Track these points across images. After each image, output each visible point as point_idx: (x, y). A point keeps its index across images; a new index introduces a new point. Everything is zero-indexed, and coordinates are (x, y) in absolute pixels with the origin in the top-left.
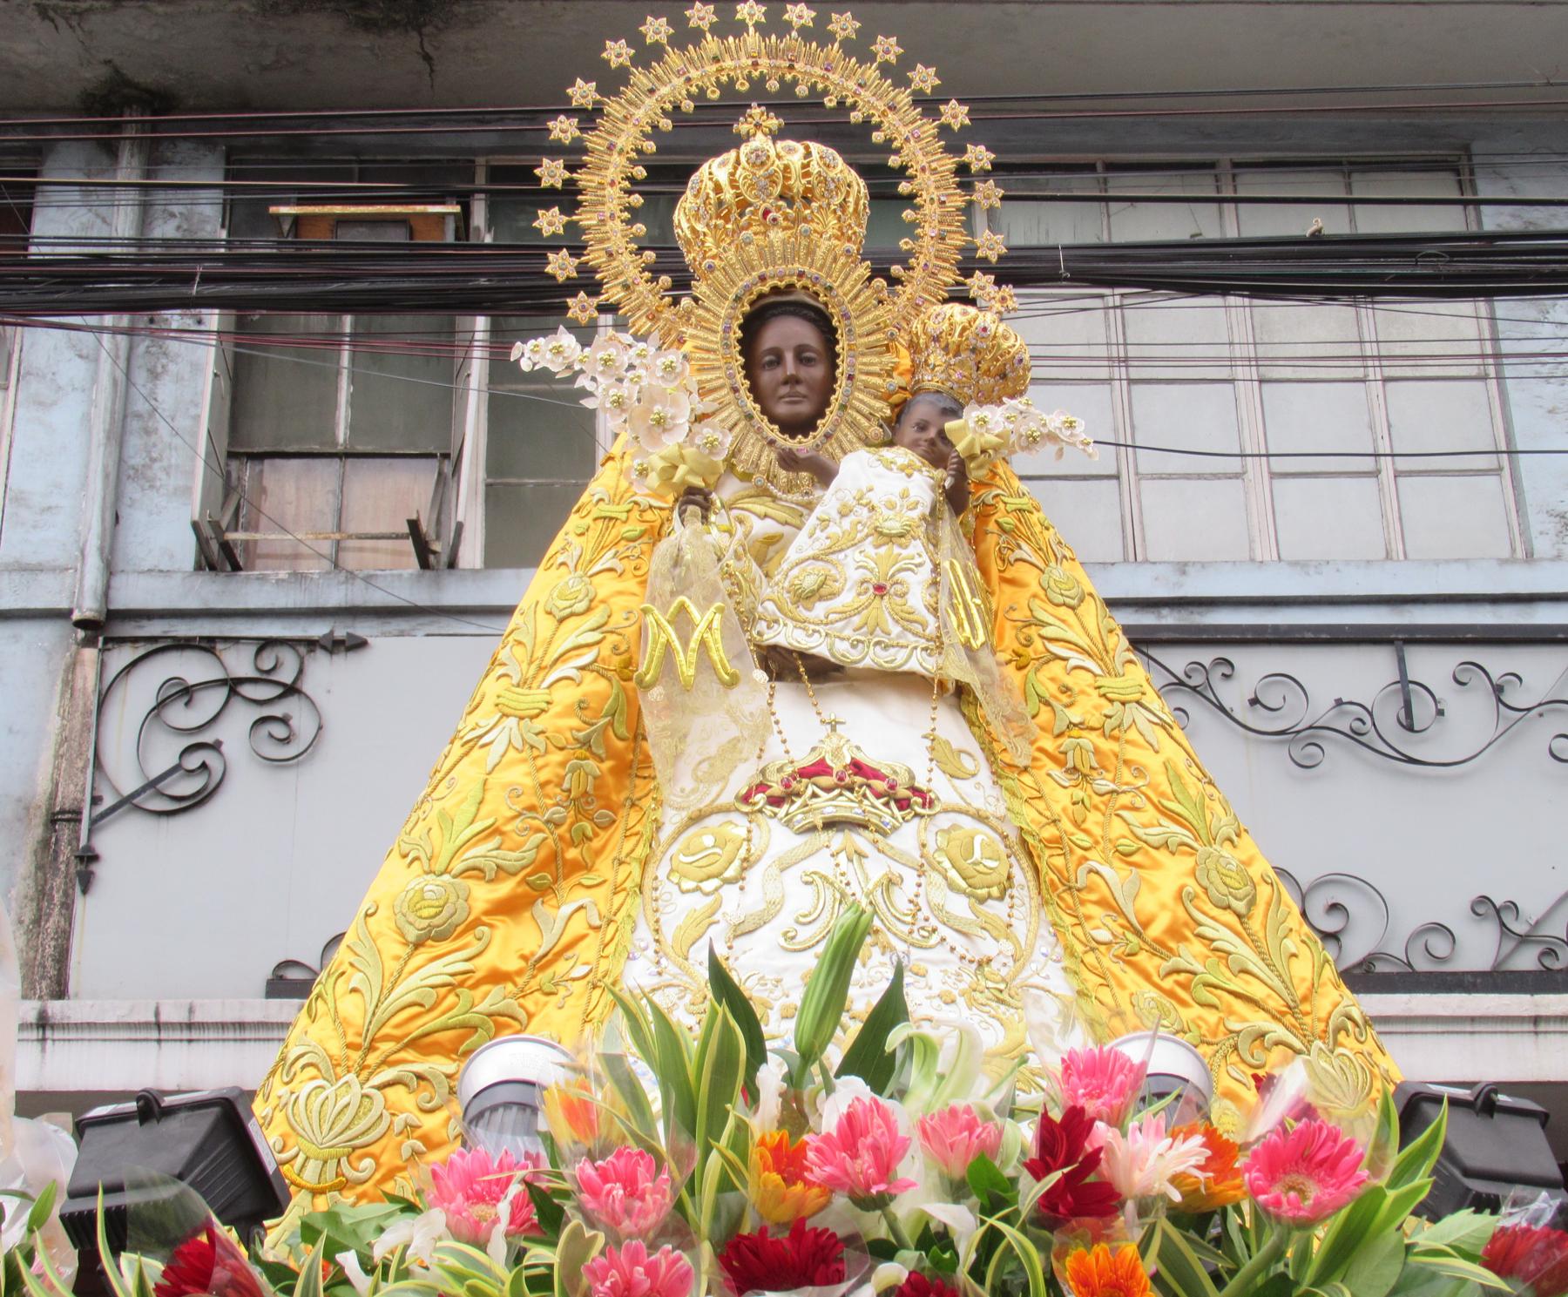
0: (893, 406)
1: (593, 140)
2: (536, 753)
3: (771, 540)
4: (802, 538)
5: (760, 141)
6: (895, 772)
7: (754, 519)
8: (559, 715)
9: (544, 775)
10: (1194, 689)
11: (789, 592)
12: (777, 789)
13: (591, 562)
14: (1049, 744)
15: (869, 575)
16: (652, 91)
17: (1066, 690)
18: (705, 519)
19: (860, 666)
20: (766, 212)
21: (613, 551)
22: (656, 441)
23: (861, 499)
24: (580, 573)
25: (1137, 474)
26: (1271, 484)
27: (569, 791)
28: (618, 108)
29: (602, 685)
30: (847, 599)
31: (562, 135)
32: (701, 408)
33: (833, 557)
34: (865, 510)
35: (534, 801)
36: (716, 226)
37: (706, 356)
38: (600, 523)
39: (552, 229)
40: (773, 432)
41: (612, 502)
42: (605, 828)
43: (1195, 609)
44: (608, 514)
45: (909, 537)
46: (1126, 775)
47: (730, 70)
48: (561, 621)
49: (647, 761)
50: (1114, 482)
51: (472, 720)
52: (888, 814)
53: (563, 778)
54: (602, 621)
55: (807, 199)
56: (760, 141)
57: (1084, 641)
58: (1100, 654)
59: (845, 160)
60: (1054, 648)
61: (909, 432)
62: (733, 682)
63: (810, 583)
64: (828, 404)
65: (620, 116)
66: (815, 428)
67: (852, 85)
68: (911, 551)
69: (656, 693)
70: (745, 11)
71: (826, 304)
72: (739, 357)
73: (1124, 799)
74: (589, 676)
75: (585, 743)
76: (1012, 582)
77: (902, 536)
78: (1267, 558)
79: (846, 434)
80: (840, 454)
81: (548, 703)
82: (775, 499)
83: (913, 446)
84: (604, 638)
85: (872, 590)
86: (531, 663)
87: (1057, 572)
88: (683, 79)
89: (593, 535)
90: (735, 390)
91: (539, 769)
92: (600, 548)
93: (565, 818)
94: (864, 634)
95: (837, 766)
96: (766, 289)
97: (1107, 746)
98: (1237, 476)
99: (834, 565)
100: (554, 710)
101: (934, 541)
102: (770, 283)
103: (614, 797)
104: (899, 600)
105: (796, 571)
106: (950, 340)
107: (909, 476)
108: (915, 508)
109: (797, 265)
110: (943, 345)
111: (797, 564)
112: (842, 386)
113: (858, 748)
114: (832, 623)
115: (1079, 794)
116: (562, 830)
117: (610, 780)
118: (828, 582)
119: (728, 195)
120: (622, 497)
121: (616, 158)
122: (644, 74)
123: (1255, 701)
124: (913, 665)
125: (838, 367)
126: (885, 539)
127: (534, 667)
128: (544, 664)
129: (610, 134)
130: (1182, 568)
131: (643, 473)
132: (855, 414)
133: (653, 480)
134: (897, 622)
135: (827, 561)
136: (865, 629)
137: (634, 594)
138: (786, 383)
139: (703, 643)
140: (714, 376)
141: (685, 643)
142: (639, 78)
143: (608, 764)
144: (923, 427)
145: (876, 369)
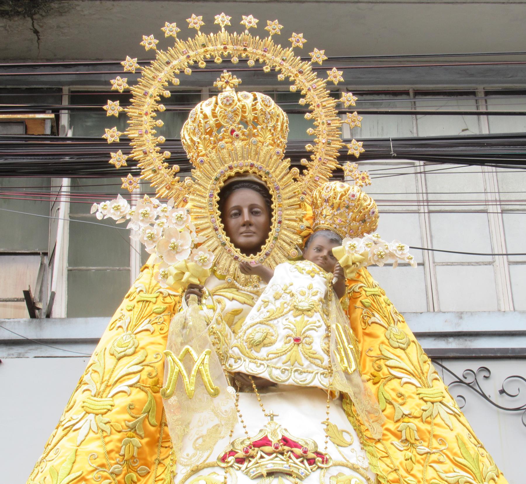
0: (303, 237)
1: (135, 90)
2: (105, 434)
3: (236, 313)
5: (228, 92)
6: (307, 443)
7: (226, 300)
8: (119, 413)
9: (110, 447)
10: (468, 384)
11: (246, 342)
12: (241, 454)
14: (392, 426)
15: (291, 333)
16: (168, 63)
17: (401, 395)
18: (200, 302)
20: (233, 131)
21: (148, 319)
22: (173, 259)
23: (286, 290)
24: (129, 332)
25: (434, 262)
26: (509, 268)
27: (124, 455)
28: (149, 72)
29: (142, 395)
30: (279, 346)
31: (118, 87)
32: (197, 241)
33: (271, 322)
35: (104, 461)
36: (204, 138)
37: (199, 210)
38: (141, 304)
39: (113, 139)
40: (237, 252)
42: (143, 476)
43: (468, 338)
44: (145, 299)
45: (313, 311)
46: (435, 443)
47: (212, 51)
48: (119, 359)
49: (167, 438)
51: (68, 415)
52: (303, 468)
53: (121, 448)
54: (142, 359)
55: (256, 122)
56: (228, 92)
57: (410, 368)
58: (419, 375)
60: (395, 372)
61: (312, 252)
62: (216, 393)
63: (258, 337)
64: (267, 237)
65: (151, 77)
66: (260, 250)
67: (278, 59)
68: (314, 319)
69: (173, 400)
70: (220, 19)
71: (266, 182)
73: (434, 457)
74: (135, 390)
75: (133, 428)
76: (369, 335)
77: (309, 310)
78: (507, 309)
79: (277, 254)
80: (274, 265)
81: (112, 406)
82: (238, 289)
84: (143, 369)
85: (292, 341)
86: (102, 383)
87: (395, 329)
88: (185, 56)
89: (137, 310)
90: (216, 230)
91: (107, 443)
92: (141, 318)
93: (121, 471)
95: (274, 440)
97: (424, 427)
98: (489, 263)
99: (272, 327)
100: (115, 410)
101: (327, 313)
102: (235, 170)
103: (149, 459)
105: (250, 331)
106: (335, 201)
107: (313, 277)
108: (316, 295)
109: (250, 161)
110: (331, 204)
111: (251, 327)
112: (275, 227)
113: (286, 430)
114: (271, 359)
115: (409, 454)
116: (120, 478)
117: (147, 449)
118: (268, 336)
119: (212, 121)
120: (153, 290)
123: (502, 392)
124: (316, 383)
126: (300, 312)
127: (104, 385)
128: (109, 384)
129: (145, 86)
130: (460, 315)
131: (165, 276)
132: (282, 242)
133: (171, 280)
137: (160, 344)
138: (244, 225)
139: (199, 372)
141: (189, 372)
142: (161, 55)
143: (146, 440)
144: (320, 249)
145: (294, 217)
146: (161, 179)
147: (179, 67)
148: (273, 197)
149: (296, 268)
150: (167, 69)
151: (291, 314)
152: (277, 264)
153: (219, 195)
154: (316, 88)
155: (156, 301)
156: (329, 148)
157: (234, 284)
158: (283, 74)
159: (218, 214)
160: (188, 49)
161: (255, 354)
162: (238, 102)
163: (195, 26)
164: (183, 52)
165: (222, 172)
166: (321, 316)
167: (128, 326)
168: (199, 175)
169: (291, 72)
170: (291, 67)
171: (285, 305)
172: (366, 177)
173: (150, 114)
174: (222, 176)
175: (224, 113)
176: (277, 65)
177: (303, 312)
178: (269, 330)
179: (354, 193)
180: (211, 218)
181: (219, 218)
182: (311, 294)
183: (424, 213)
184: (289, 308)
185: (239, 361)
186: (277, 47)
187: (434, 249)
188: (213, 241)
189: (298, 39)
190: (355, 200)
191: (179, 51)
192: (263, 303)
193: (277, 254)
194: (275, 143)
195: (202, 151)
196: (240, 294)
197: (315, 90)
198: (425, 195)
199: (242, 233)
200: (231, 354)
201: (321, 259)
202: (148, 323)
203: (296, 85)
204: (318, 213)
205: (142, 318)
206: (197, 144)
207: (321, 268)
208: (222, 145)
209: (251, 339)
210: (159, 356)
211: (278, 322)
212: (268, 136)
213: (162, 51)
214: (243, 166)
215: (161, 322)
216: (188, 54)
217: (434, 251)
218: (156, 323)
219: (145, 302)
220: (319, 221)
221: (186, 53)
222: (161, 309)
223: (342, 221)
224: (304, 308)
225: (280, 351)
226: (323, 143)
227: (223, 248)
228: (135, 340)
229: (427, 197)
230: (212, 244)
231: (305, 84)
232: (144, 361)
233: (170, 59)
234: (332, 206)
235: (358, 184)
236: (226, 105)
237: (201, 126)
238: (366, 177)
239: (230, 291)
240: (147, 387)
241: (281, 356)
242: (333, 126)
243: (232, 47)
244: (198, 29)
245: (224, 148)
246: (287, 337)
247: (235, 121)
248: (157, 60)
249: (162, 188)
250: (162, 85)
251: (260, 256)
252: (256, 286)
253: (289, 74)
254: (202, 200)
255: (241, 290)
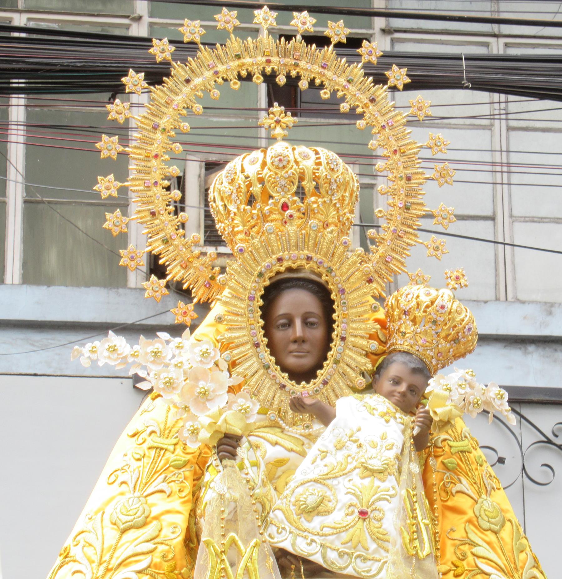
3: (280, 463)
4: (306, 463)
11: (294, 505)
13: (146, 484)
15: (355, 501)
16: (188, 81)
19: (345, 572)
21: (163, 476)
23: (351, 436)
24: (137, 494)
25: (511, 216)
31: (118, 116)
33: (329, 482)
34: (355, 446)
37: (236, 318)
38: (153, 452)
39: (108, 193)
41: (162, 435)
44: (160, 445)
45: (386, 473)
47: (249, 65)
48: (123, 531)
50: (490, 223)
54: (154, 535)
59: (343, 161)
61: (387, 385)
63: (311, 501)
64: (326, 359)
65: (163, 101)
66: (315, 377)
67: (342, 81)
70: (261, 17)
71: (327, 282)
72: (261, 320)
77: (381, 472)
79: (339, 383)
82: (283, 430)
83: (389, 395)
84: (156, 548)
85: (357, 513)
86: (100, 564)
88: (212, 72)
89: (147, 461)
90: (257, 345)
94: (349, 548)
96: (282, 269)
99: (330, 489)
102: (286, 264)
104: (377, 524)
105: (300, 490)
106: (418, 314)
107: (387, 421)
108: (391, 449)
109: (306, 252)
110: (412, 318)
111: (302, 484)
112: (336, 346)
114: (326, 535)
118: (325, 502)
120: (170, 432)
121: (159, 136)
122: (182, 68)
125: (333, 330)
126: (368, 473)
128: (110, 567)
132: (345, 367)
134: (374, 540)
135: (324, 485)
136: (349, 544)
138: (295, 341)
140: (241, 334)
144: (397, 381)
145: (362, 333)
146: (174, 253)
147: (203, 88)
148: (336, 304)
149: (365, 406)
150: (186, 90)
151: (357, 474)
152: (337, 397)
153: (262, 297)
154: (392, 125)
155: (174, 450)
156: (407, 215)
157: (278, 423)
158: (347, 102)
159: (260, 324)
160: (216, 61)
161: (306, 525)
162: (294, 164)
163: (227, 26)
164: (209, 66)
165: (268, 266)
166: (397, 481)
167: (135, 484)
168: (237, 270)
169: (359, 101)
170: (359, 92)
171: (350, 460)
172: (461, 276)
173: (162, 156)
174: (268, 272)
175: (274, 178)
176: (340, 88)
177: (374, 473)
178: (326, 493)
179: (444, 304)
180: (252, 329)
181: (261, 330)
182: (384, 447)
183: (502, 184)
184: (355, 464)
185: (284, 532)
186: (341, 61)
187: (515, 243)
188: (252, 362)
189: (371, 51)
190: (444, 313)
191: (203, 64)
192: (319, 453)
193: (339, 383)
194: (339, 221)
195: (238, 226)
196: (286, 437)
197: (390, 128)
198: (504, 154)
199: (291, 352)
200: (273, 518)
201: (399, 395)
202: (163, 481)
203: (365, 120)
204: (394, 329)
205: (155, 473)
206: (232, 215)
207: (397, 407)
208: (270, 229)
209: (302, 503)
210: (177, 530)
211: (339, 483)
212: (331, 213)
213: (179, 63)
214: (297, 259)
215: (181, 480)
216: (216, 69)
217: (515, 248)
218: (174, 481)
219: (158, 450)
220: (396, 339)
221: (213, 67)
222: (181, 462)
223: (428, 342)
224: (375, 468)
225: (340, 526)
226: (400, 208)
227: (266, 372)
228: (145, 506)
229: (508, 158)
230: (250, 366)
231: (378, 119)
232: (157, 536)
233: (191, 75)
234: (414, 321)
235: (451, 286)
236: (278, 168)
237: (241, 192)
238: (461, 276)
239: (272, 432)
240: (161, 574)
241: (340, 532)
242: (414, 183)
243: (278, 59)
244: (231, 31)
245: (271, 233)
246: (350, 506)
247: (289, 190)
248: (172, 77)
249: (176, 266)
250: (179, 114)
251: (314, 384)
252: (308, 427)
253: (357, 103)
254: (240, 304)
255: (288, 431)
